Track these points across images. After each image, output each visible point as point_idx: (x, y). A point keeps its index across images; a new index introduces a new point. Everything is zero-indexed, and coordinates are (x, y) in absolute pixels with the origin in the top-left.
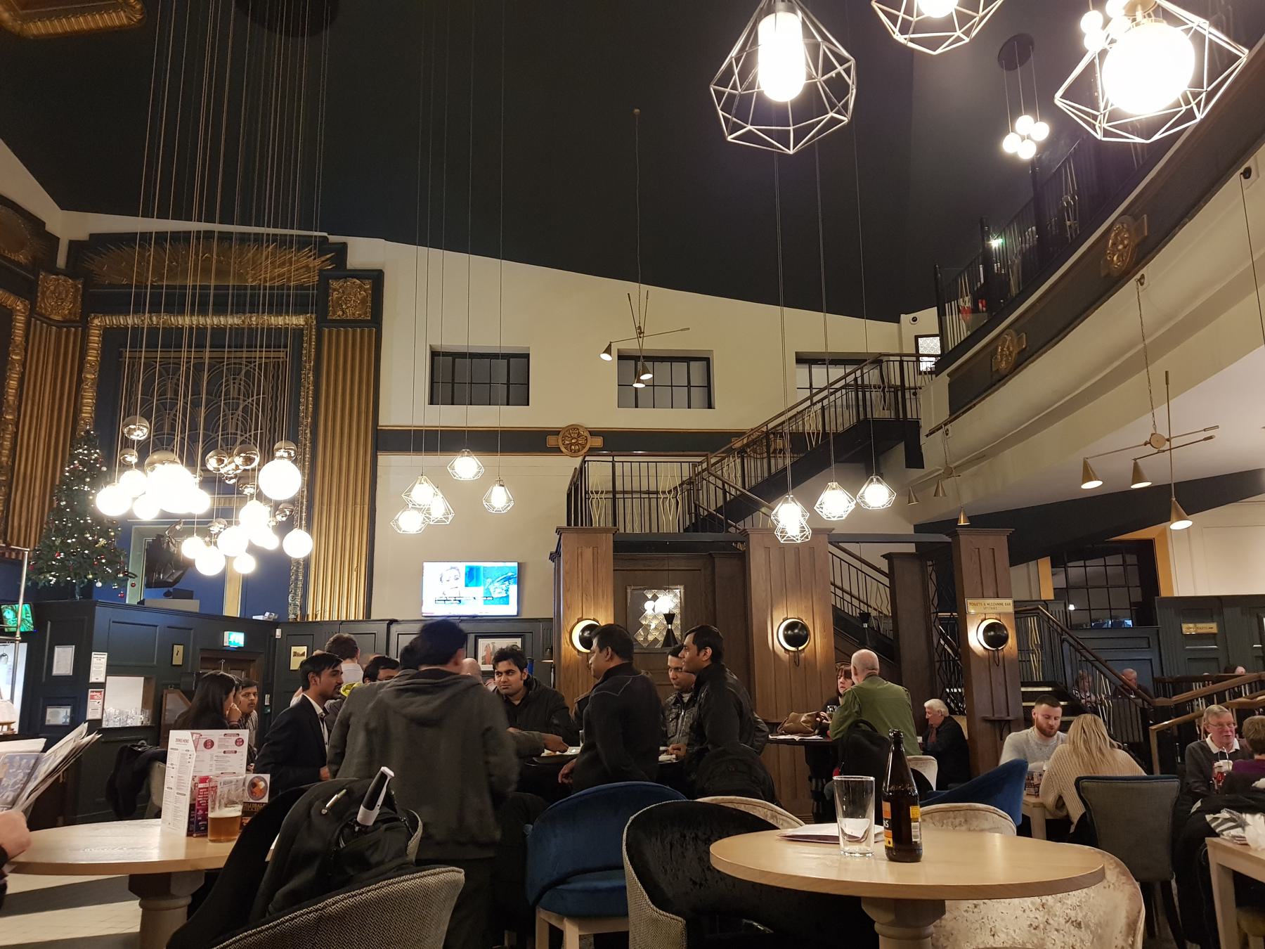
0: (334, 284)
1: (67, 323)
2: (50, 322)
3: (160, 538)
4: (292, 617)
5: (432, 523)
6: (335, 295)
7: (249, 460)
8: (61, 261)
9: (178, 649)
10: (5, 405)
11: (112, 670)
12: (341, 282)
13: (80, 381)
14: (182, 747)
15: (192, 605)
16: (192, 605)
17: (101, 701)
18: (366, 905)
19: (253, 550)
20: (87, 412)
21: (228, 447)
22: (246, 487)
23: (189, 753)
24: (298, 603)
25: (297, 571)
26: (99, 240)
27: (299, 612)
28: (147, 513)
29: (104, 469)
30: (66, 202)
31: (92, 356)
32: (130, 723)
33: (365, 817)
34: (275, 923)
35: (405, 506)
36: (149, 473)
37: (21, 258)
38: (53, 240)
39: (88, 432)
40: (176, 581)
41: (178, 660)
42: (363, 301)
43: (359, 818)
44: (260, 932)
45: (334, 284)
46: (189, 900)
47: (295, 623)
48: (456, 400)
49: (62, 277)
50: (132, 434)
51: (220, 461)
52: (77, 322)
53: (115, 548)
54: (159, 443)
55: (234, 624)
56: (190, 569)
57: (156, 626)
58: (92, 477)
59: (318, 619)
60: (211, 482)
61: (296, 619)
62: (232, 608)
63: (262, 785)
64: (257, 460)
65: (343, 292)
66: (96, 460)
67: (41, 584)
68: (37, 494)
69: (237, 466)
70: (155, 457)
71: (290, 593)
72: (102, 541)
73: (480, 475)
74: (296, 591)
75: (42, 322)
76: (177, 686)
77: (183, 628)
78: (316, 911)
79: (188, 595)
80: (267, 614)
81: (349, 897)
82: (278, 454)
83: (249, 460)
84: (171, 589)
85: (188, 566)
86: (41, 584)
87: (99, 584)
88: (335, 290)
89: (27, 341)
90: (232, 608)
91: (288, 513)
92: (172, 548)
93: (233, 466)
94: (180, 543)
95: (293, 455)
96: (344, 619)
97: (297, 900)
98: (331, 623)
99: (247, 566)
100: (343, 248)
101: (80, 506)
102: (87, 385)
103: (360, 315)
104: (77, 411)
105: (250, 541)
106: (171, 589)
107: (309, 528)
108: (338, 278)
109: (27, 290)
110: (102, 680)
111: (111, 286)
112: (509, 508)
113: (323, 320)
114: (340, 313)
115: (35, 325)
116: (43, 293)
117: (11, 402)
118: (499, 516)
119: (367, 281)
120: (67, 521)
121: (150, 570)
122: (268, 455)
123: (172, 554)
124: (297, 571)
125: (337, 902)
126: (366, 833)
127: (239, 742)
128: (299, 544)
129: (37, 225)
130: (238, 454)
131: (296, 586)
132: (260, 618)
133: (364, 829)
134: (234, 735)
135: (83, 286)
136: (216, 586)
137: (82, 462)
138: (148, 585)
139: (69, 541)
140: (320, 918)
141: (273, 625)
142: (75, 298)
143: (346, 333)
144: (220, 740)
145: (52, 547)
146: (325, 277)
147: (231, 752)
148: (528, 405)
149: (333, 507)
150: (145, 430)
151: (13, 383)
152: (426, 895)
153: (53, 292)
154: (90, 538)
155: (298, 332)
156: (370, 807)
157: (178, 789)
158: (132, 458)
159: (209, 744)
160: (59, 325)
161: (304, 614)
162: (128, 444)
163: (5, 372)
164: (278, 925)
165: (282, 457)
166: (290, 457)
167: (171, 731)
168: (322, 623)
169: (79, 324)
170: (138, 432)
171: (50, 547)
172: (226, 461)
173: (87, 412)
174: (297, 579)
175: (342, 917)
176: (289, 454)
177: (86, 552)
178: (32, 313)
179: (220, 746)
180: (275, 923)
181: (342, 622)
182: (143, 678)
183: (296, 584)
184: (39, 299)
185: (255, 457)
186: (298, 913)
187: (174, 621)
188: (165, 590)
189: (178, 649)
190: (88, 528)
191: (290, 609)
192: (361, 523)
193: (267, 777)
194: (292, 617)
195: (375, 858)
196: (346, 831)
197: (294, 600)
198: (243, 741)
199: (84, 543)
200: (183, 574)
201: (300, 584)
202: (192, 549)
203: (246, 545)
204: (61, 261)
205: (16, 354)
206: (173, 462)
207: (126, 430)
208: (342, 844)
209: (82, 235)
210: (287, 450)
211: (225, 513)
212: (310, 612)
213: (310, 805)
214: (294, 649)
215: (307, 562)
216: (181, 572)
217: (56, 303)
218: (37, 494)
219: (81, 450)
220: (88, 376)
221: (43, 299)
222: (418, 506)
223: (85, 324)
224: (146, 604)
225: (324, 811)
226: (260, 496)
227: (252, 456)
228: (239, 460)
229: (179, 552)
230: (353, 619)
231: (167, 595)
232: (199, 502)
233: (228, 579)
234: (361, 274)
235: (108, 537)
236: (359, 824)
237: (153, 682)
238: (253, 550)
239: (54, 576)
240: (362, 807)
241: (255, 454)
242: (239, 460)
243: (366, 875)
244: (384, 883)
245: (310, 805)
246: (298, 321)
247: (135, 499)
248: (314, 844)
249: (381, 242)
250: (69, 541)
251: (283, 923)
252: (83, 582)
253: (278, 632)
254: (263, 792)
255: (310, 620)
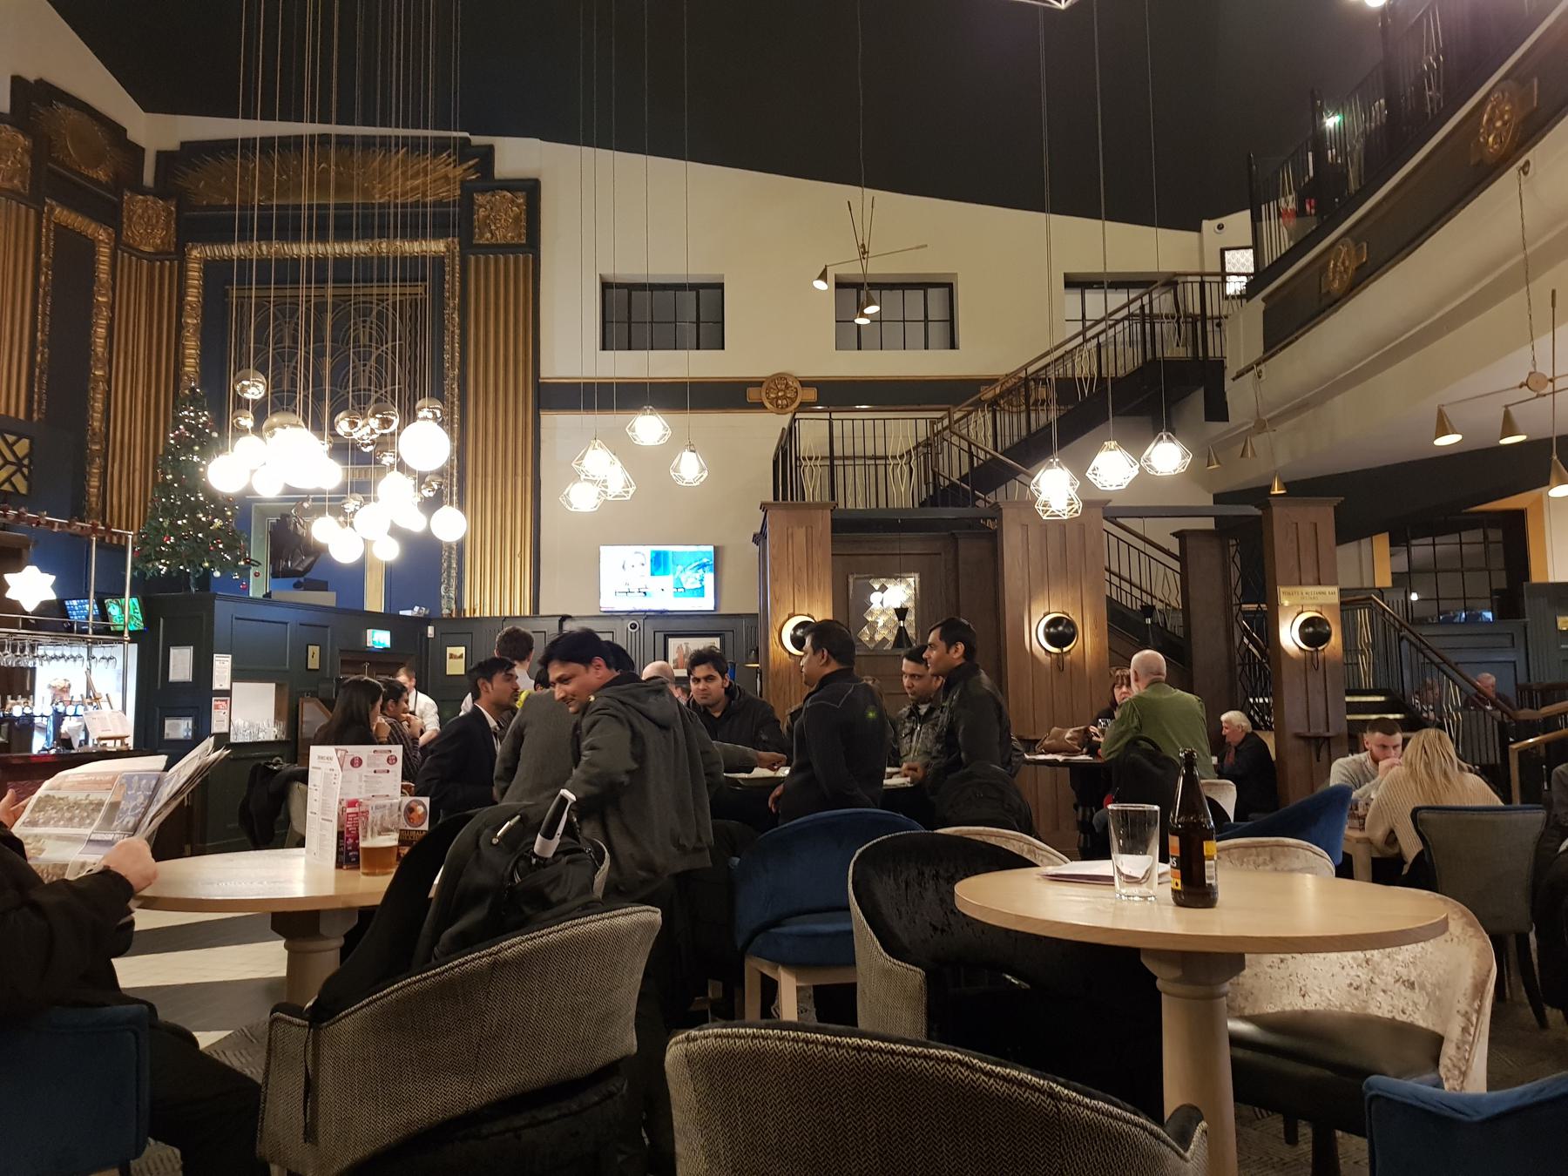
0: (480, 199)
1: (160, 255)
2: (133, 250)
3: (285, 517)
4: (445, 611)
5: (609, 498)
6: (482, 212)
7: (386, 422)
8: (148, 177)
9: (314, 650)
10: (93, 358)
11: (238, 675)
12: (488, 196)
13: (180, 327)
14: (325, 766)
15: (327, 599)
16: (327, 599)
17: (227, 712)
18: (548, 949)
19: (395, 532)
20: (191, 365)
21: (360, 407)
22: (385, 456)
23: (333, 773)
24: (452, 595)
25: (449, 557)
26: (194, 151)
27: (454, 607)
28: (269, 489)
29: (215, 435)
30: (151, 101)
31: (193, 296)
32: (262, 737)
33: (543, 847)
34: (443, 968)
35: (575, 477)
36: (268, 439)
37: (101, 175)
38: (138, 152)
39: (193, 390)
40: (307, 570)
41: (314, 663)
42: (517, 219)
43: (536, 848)
44: (425, 979)
45: (480, 199)
46: (340, 942)
47: (449, 618)
48: (633, 345)
49: (150, 198)
50: (246, 392)
51: (353, 424)
52: (170, 253)
53: (233, 531)
54: (279, 402)
55: (378, 621)
56: (322, 555)
57: (286, 623)
58: (201, 445)
59: (477, 615)
60: (343, 450)
61: (451, 615)
62: (375, 602)
63: (420, 809)
64: (396, 421)
65: (492, 209)
66: (205, 424)
67: (149, 574)
68: (138, 466)
69: (372, 430)
70: (275, 419)
71: (441, 584)
72: (218, 523)
73: (667, 438)
74: (449, 581)
75: (131, 255)
76: (314, 694)
77: (318, 625)
78: (490, 955)
79: (322, 586)
80: (416, 608)
81: (527, 940)
82: (421, 414)
83: (386, 422)
84: (302, 579)
85: (319, 552)
86: (149, 574)
87: (217, 574)
88: (481, 206)
89: (114, 279)
90: (375, 602)
91: (436, 487)
92: (301, 531)
93: (367, 429)
94: (309, 524)
95: (439, 415)
96: (507, 614)
97: (466, 942)
98: (492, 619)
99: (389, 552)
100: (488, 153)
101: (191, 481)
102: (188, 331)
103: (512, 238)
104: (179, 364)
105: (392, 522)
106: (302, 579)
107: (461, 506)
108: (483, 191)
109: (111, 216)
110: (226, 686)
111: (209, 207)
112: (702, 480)
113: (468, 246)
114: (488, 235)
115: (123, 257)
116: (130, 219)
117: (100, 355)
118: (689, 490)
119: (520, 194)
120: (175, 499)
121: (275, 556)
122: (409, 416)
123: (301, 537)
124: (449, 557)
125: (513, 946)
126: (545, 866)
127: (392, 760)
128: (450, 525)
129: (116, 131)
130: (373, 416)
131: (449, 576)
132: (408, 613)
133: (543, 862)
134: (385, 752)
135: (177, 207)
136: (355, 575)
137: (189, 428)
138: (275, 575)
139: (180, 522)
140: (494, 966)
141: (424, 621)
142: (168, 224)
143: (497, 261)
144: (369, 757)
145: (159, 530)
146: (468, 190)
147: (383, 771)
148: (723, 348)
149: (489, 480)
150: (261, 387)
151: (101, 331)
152: (617, 938)
153: (141, 217)
154: (201, 515)
155: (439, 261)
156: (549, 835)
157: (322, 814)
158: (247, 421)
159: (357, 763)
160: (152, 258)
161: (460, 609)
162: (241, 404)
163: (90, 317)
164: (447, 970)
165: (425, 418)
166: (435, 418)
167: (312, 747)
168: (481, 619)
169: (175, 256)
170: (253, 389)
171: (156, 528)
172: (360, 423)
173: (191, 365)
174: (450, 566)
175: (521, 963)
176: (434, 414)
177: (200, 535)
178: (118, 243)
179: (368, 765)
180: (443, 968)
181: (506, 618)
182: (273, 685)
183: (449, 573)
184: (125, 226)
185: (393, 418)
186: (469, 957)
187: (304, 617)
188: (296, 580)
189: (314, 650)
190: (200, 506)
191: (443, 602)
192: (524, 499)
193: (426, 800)
194: (445, 611)
195: (555, 896)
196: (522, 864)
197: (447, 592)
198: (396, 759)
199: (196, 525)
200: (314, 561)
201: (454, 573)
202: (323, 530)
203: (387, 527)
204: (148, 177)
205: (102, 295)
206: (297, 425)
207: (238, 388)
208: (517, 879)
209: (172, 144)
210: (431, 410)
211: (362, 488)
212: (467, 606)
213: (478, 835)
214: (450, 650)
215: (461, 546)
216: (311, 559)
217: (145, 230)
218: (138, 466)
219: (186, 413)
220: (189, 321)
221: (130, 226)
222: (591, 478)
223: (181, 257)
224: (274, 597)
225: (495, 841)
226: (401, 466)
227: (390, 417)
228: (374, 423)
229: (309, 534)
230: (518, 614)
231: (297, 586)
232: (328, 474)
233: (367, 566)
234: (512, 185)
235: (224, 518)
236: (535, 856)
237: (287, 689)
238: (395, 532)
239: (165, 564)
240: (539, 836)
241: (393, 415)
242: (374, 423)
243: (547, 915)
244: (568, 923)
245: (478, 835)
246: (437, 247)
247: (253, 472)
248: (482, 878)
249: (535, 143)
250: (180, 522)
251: (452, 968)
252: (198, 571)
253: (431, 630)
254: (422, 818)
255: (468, 615)
